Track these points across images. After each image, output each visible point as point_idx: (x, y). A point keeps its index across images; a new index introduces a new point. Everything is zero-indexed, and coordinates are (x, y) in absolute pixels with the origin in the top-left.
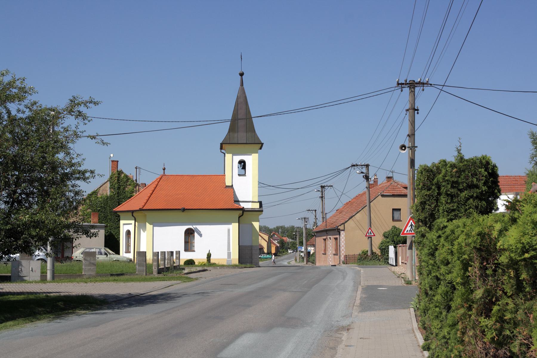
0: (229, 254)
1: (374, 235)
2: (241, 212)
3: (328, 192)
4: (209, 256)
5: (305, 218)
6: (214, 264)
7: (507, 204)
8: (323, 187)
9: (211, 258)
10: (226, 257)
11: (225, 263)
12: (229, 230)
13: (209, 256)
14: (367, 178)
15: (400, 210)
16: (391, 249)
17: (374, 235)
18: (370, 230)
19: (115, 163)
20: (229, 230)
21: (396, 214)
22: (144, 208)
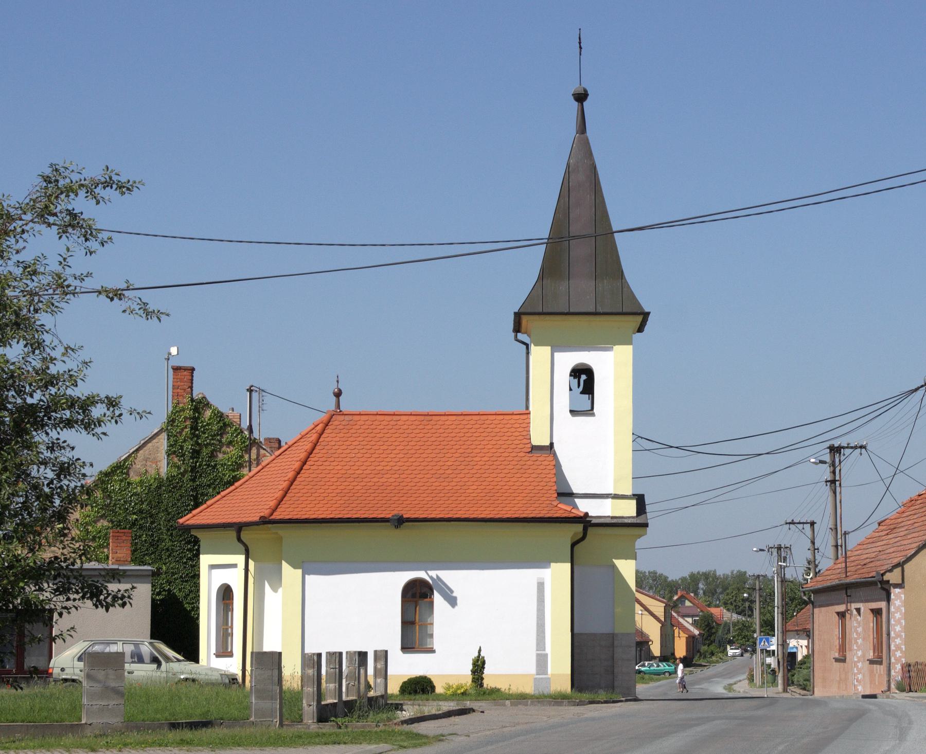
0: (542, 661)
5: (779, 548)
6: (495, 692)
8: (835, 450)
10: (531, 668)
12: (541, 586)
20: (541, 586)
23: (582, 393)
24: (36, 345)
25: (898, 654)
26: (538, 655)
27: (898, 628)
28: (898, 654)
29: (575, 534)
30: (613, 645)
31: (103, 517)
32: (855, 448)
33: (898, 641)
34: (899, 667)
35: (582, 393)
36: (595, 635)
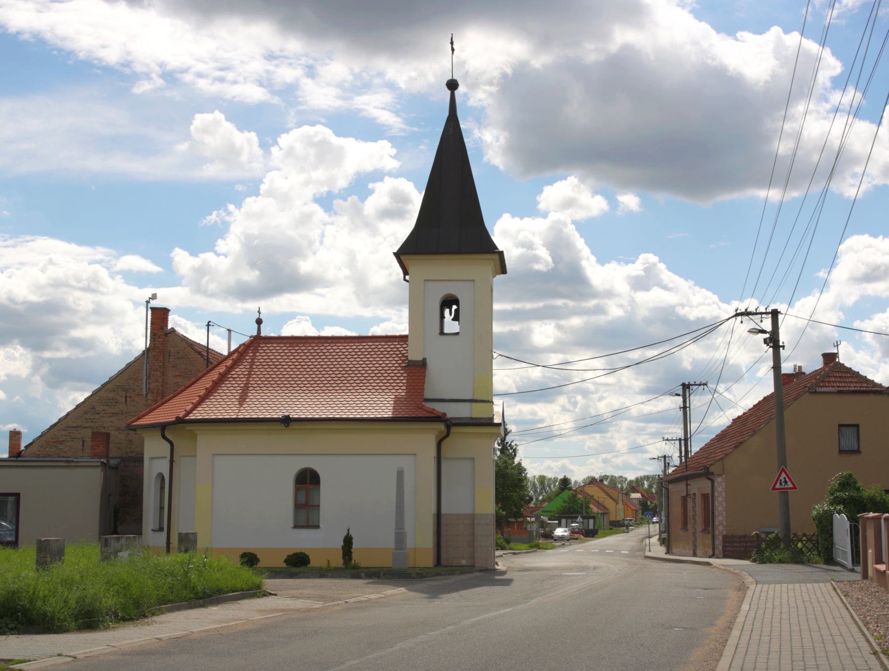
0: (400, 538)
1: (795, 488)
2: (442, 427)
3: (697, 401)
4: (348, 541)
5: (665, 457)
6: (356, 567)
7: (497, 577)
8: (686, 387)
9: (354, 546)
10: (389, 542)
11: (387, 562)
12: (400, 474)
13: (348, 541)
14: (773, 341)
15: (841, 452)
16: (841, 522)
17: (795, 488)
18: (783, 475)
19: (159, 316)
20: (400, 474)
21: (849, 442)
22: (191, 417)
23: (453, 320)
24: (352, 70)
25: (721, 528)
26: (396, 533)
27: (720, 508)
28: (721, 528)
29: (440, 432)
30: (473, 524)
31: (529, 522)
32: (700, 385)
33: (720, 518)
34: (721, 538)
35: (453, 320)
36: (458, 515)
